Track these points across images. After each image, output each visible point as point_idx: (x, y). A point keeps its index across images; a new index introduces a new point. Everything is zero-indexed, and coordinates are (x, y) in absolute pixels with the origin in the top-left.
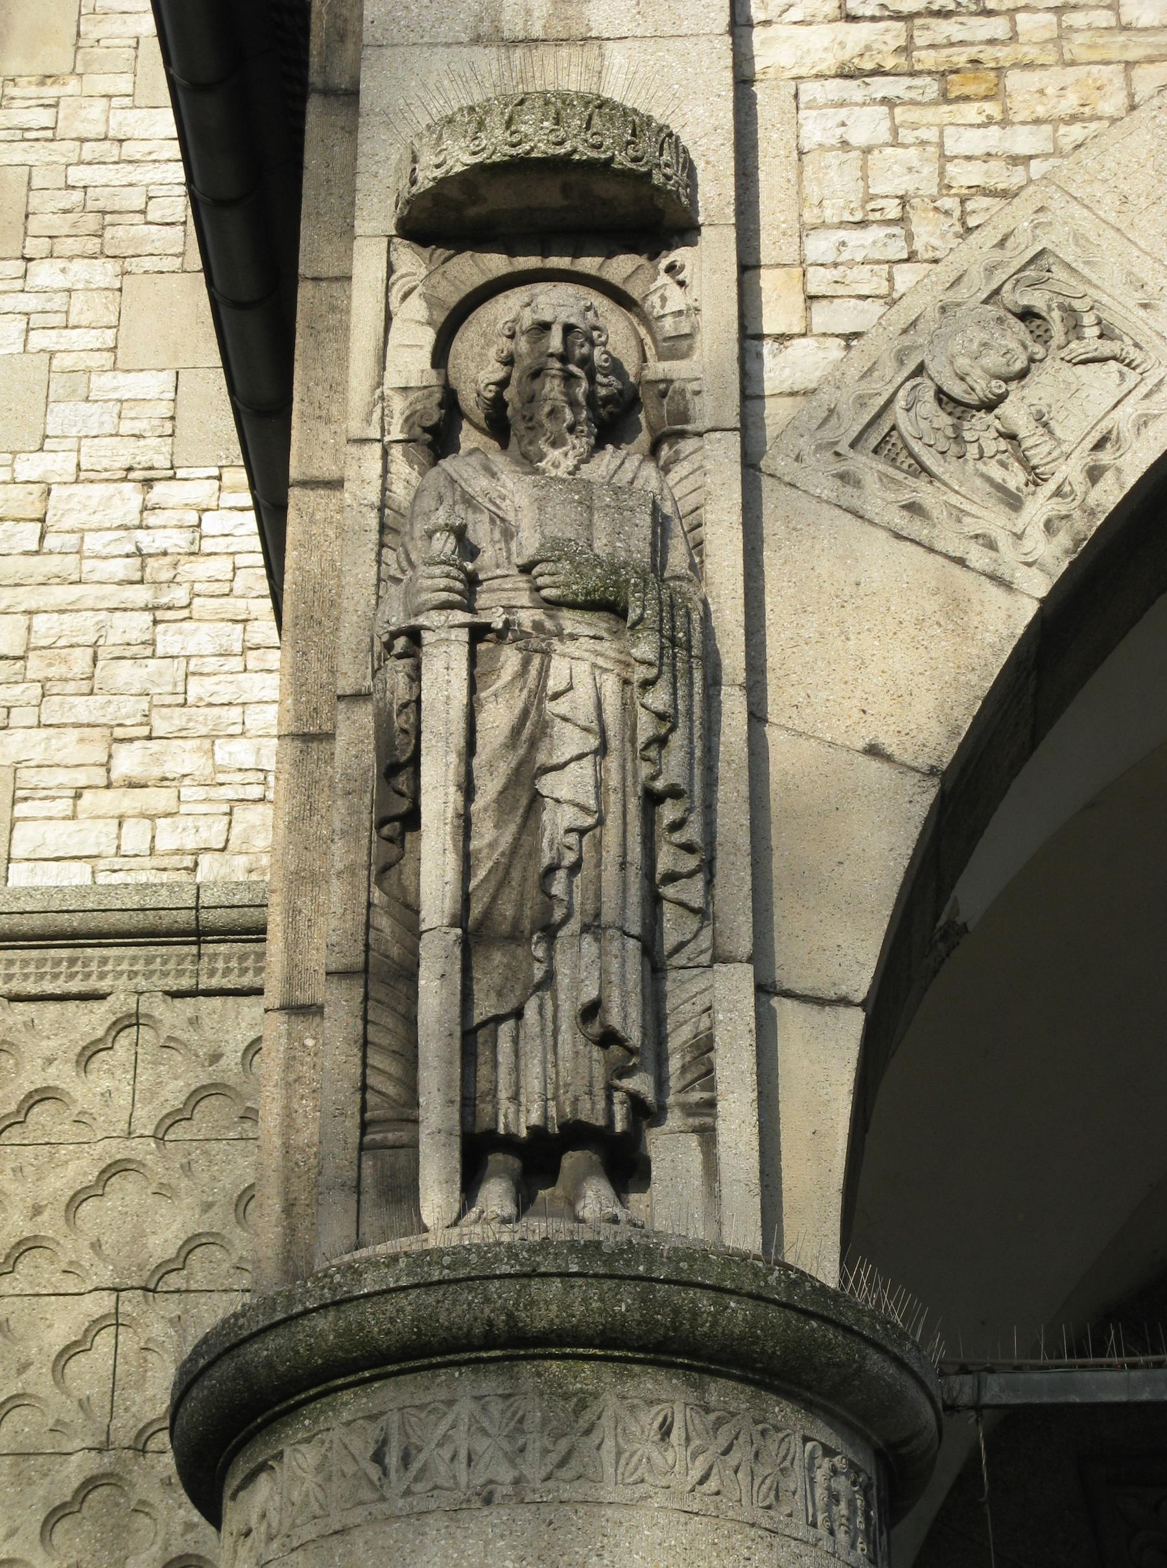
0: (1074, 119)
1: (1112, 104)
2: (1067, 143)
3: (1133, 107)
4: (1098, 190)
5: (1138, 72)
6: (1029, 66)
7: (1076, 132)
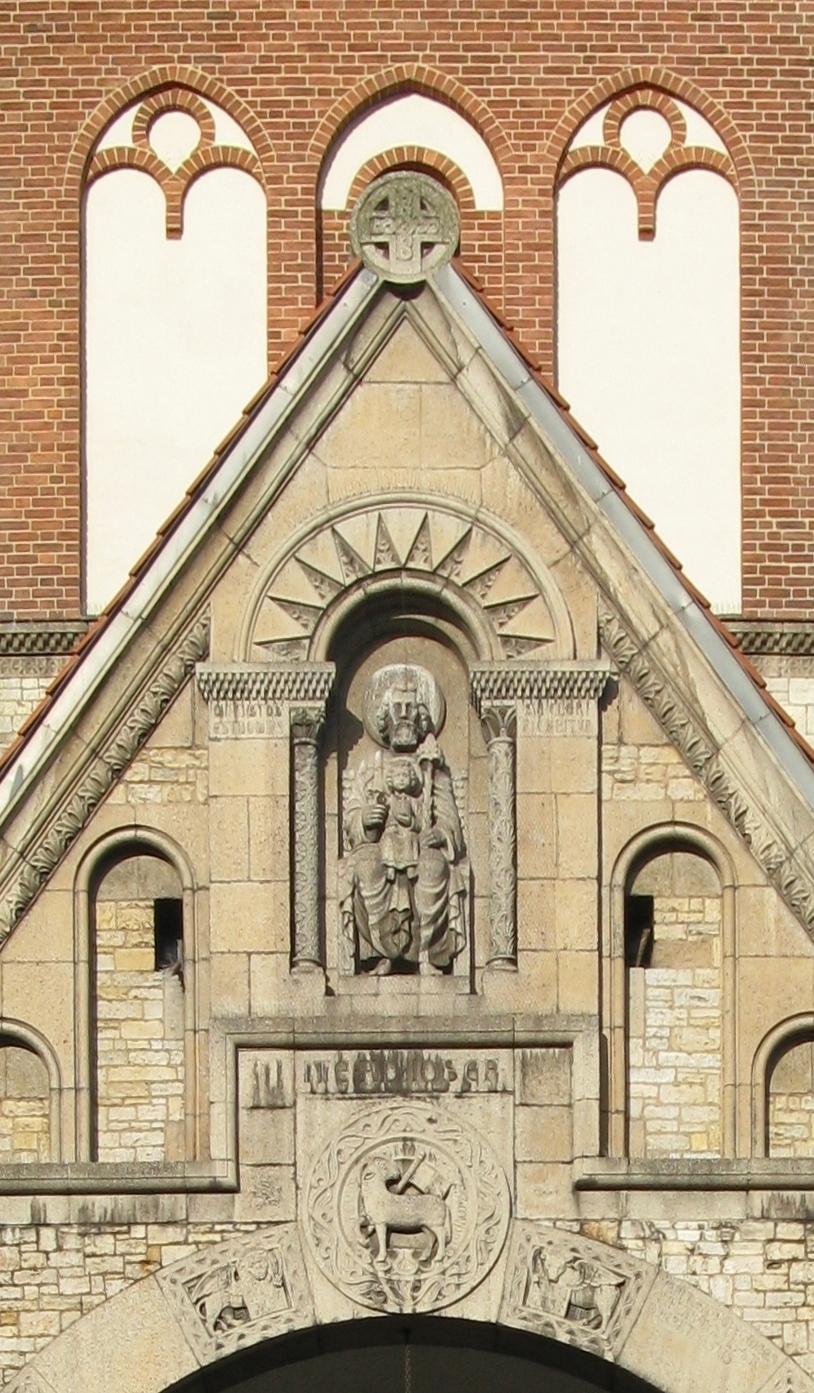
0: (42, 1336)
1: (53, 1331)
2: (38, 1347)
3: (61, 1331)
4: (47, 1370)
5: (65, 1315)
6: (28, 1311)
7: (41, 1342)
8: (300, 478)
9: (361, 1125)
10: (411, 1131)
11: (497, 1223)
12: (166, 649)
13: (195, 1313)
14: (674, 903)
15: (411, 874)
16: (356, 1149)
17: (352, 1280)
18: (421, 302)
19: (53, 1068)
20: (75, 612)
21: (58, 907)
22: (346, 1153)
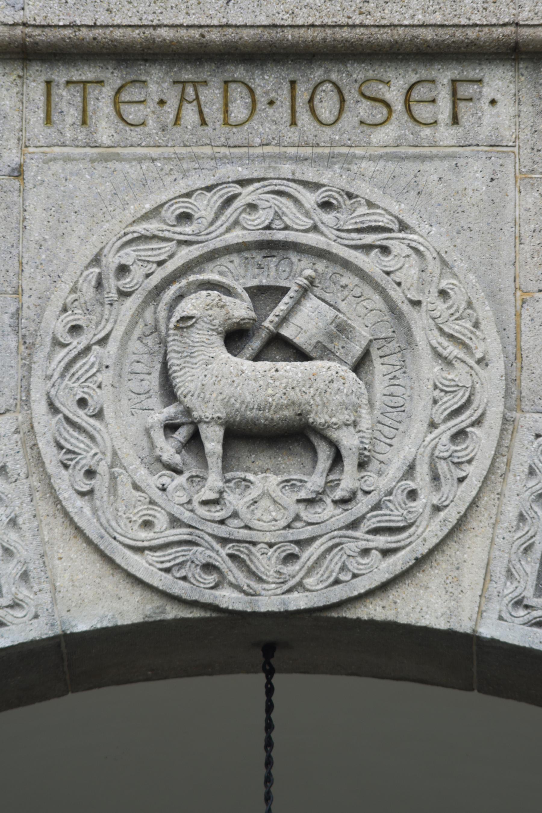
9: (169, 214)
10: (286, 228)
11: (478, 422)
16: (160, 263)
17: (144, 537)
22: (137, 272)
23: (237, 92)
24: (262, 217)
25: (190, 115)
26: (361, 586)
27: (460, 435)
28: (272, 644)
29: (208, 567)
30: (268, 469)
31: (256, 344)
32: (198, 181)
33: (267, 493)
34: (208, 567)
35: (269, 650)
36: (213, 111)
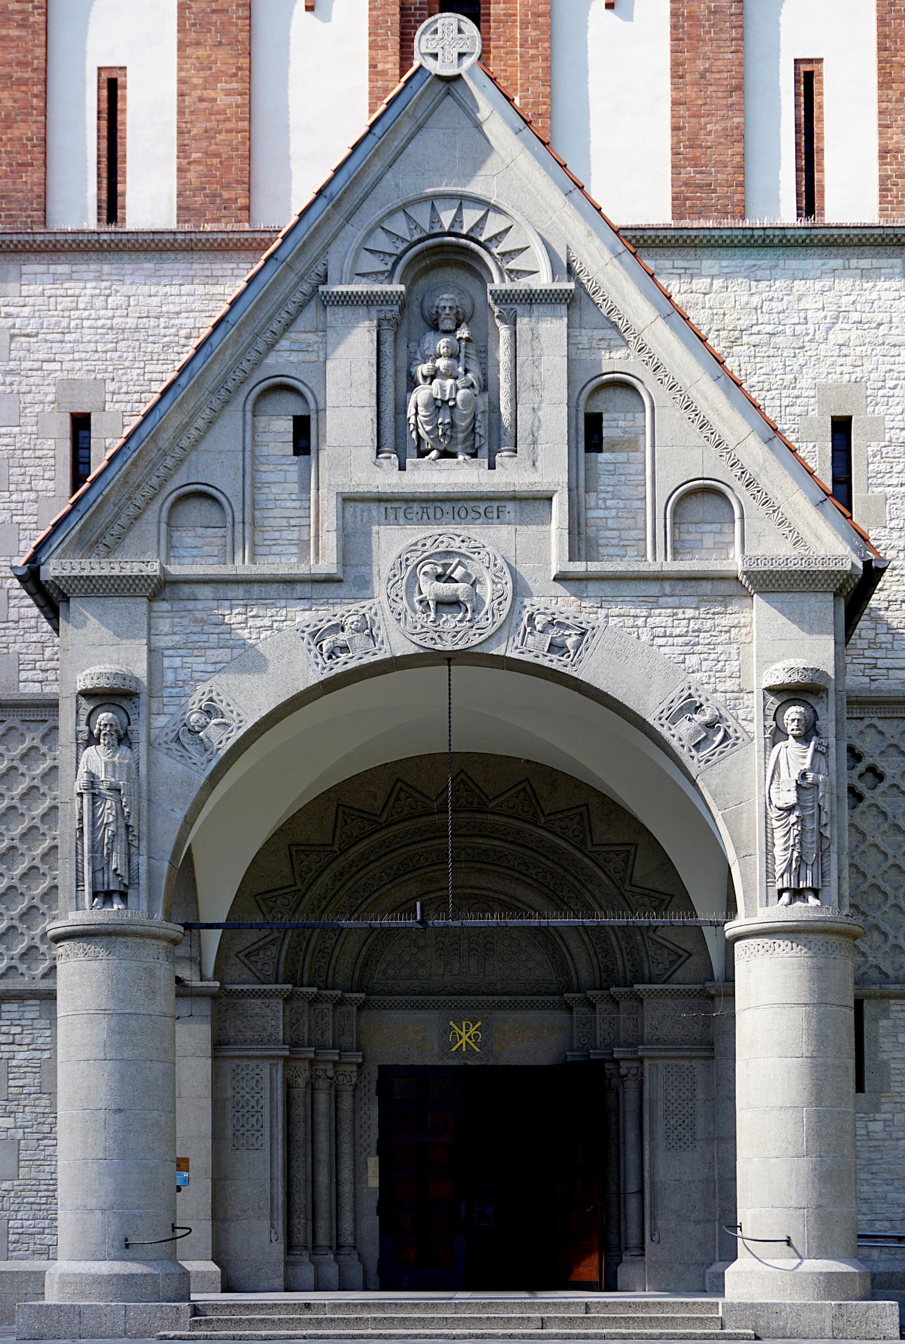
8: (384, 182)
9: (420, 544)
12: (302, 278)
13: (316, 650)
14: (616, 415)
15: (451, 403)
17: (414, 631)
18: (457, 86)
19: (229, 511)
20: (246, 227)
21: (233, 422)
23: (438, 510)
24: (445, 544)
25: (425, 517)
26: (474, 643)
27: (500, 603)
28: (449, 658)
29: (432, 639)
30: (863, 834)
31: (444, 579)
32: (427, 534)
33: (450, 621)
34: (432, 639)
35: (449, 660)
36: (431, 515)
